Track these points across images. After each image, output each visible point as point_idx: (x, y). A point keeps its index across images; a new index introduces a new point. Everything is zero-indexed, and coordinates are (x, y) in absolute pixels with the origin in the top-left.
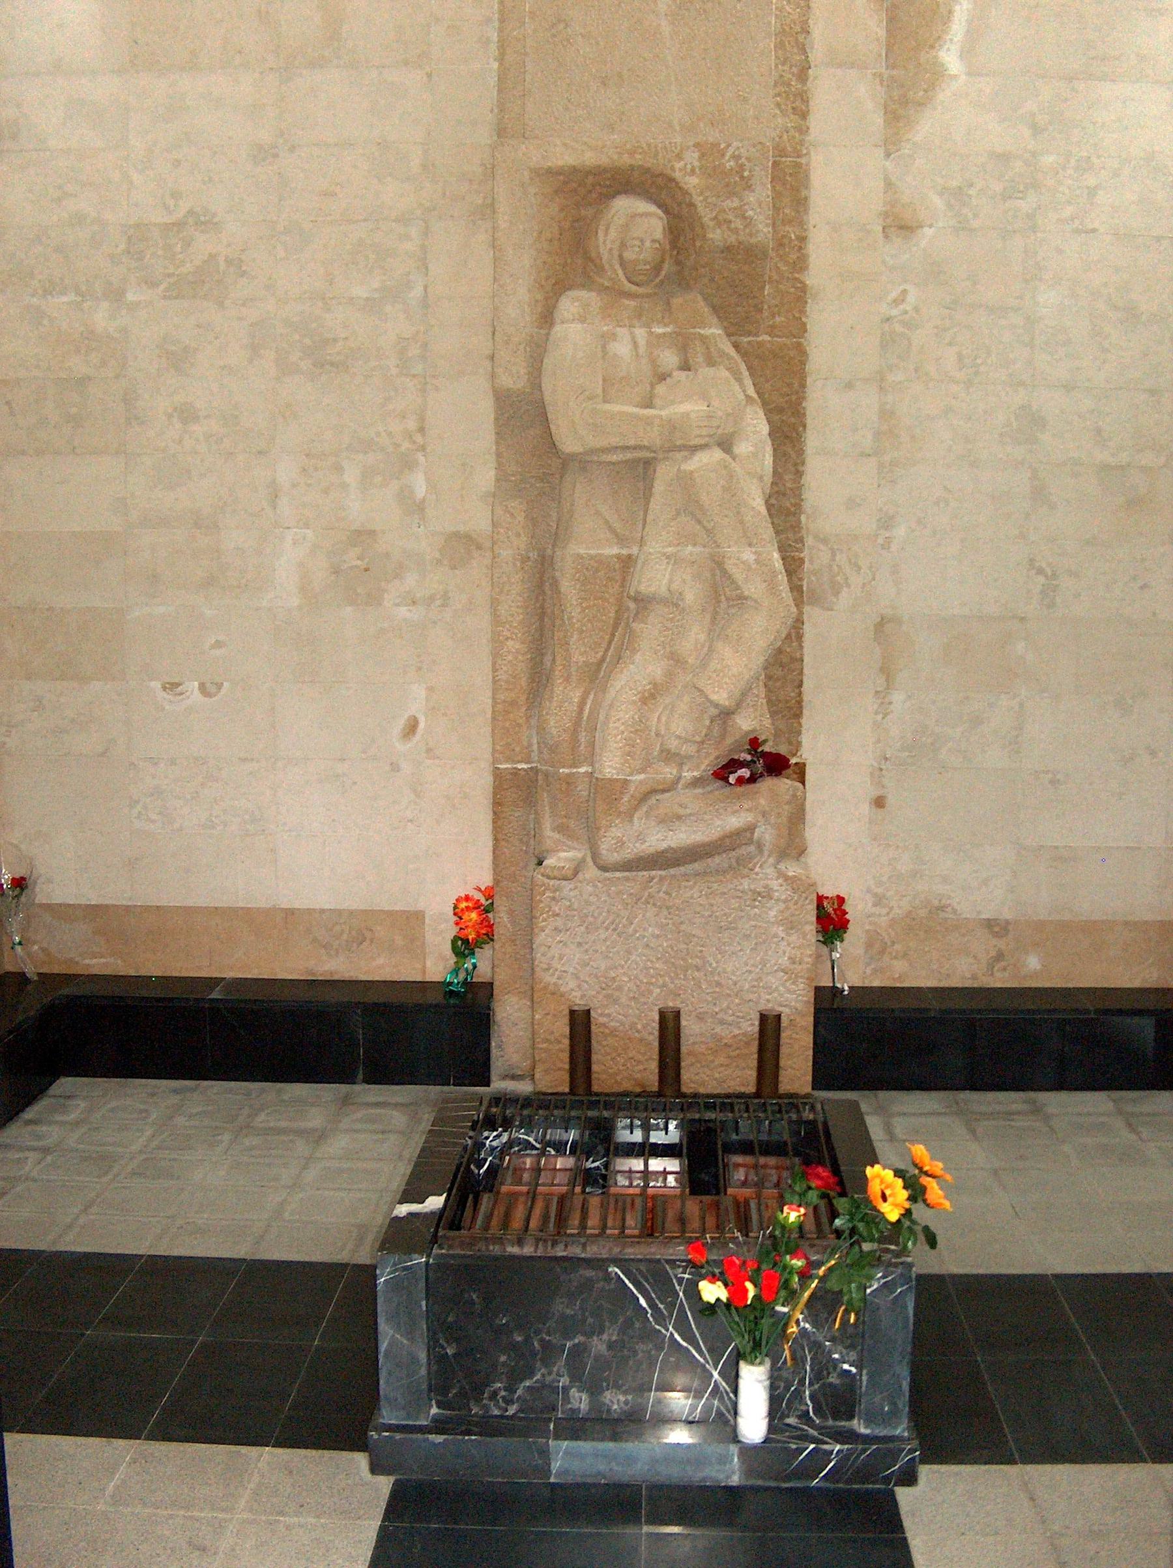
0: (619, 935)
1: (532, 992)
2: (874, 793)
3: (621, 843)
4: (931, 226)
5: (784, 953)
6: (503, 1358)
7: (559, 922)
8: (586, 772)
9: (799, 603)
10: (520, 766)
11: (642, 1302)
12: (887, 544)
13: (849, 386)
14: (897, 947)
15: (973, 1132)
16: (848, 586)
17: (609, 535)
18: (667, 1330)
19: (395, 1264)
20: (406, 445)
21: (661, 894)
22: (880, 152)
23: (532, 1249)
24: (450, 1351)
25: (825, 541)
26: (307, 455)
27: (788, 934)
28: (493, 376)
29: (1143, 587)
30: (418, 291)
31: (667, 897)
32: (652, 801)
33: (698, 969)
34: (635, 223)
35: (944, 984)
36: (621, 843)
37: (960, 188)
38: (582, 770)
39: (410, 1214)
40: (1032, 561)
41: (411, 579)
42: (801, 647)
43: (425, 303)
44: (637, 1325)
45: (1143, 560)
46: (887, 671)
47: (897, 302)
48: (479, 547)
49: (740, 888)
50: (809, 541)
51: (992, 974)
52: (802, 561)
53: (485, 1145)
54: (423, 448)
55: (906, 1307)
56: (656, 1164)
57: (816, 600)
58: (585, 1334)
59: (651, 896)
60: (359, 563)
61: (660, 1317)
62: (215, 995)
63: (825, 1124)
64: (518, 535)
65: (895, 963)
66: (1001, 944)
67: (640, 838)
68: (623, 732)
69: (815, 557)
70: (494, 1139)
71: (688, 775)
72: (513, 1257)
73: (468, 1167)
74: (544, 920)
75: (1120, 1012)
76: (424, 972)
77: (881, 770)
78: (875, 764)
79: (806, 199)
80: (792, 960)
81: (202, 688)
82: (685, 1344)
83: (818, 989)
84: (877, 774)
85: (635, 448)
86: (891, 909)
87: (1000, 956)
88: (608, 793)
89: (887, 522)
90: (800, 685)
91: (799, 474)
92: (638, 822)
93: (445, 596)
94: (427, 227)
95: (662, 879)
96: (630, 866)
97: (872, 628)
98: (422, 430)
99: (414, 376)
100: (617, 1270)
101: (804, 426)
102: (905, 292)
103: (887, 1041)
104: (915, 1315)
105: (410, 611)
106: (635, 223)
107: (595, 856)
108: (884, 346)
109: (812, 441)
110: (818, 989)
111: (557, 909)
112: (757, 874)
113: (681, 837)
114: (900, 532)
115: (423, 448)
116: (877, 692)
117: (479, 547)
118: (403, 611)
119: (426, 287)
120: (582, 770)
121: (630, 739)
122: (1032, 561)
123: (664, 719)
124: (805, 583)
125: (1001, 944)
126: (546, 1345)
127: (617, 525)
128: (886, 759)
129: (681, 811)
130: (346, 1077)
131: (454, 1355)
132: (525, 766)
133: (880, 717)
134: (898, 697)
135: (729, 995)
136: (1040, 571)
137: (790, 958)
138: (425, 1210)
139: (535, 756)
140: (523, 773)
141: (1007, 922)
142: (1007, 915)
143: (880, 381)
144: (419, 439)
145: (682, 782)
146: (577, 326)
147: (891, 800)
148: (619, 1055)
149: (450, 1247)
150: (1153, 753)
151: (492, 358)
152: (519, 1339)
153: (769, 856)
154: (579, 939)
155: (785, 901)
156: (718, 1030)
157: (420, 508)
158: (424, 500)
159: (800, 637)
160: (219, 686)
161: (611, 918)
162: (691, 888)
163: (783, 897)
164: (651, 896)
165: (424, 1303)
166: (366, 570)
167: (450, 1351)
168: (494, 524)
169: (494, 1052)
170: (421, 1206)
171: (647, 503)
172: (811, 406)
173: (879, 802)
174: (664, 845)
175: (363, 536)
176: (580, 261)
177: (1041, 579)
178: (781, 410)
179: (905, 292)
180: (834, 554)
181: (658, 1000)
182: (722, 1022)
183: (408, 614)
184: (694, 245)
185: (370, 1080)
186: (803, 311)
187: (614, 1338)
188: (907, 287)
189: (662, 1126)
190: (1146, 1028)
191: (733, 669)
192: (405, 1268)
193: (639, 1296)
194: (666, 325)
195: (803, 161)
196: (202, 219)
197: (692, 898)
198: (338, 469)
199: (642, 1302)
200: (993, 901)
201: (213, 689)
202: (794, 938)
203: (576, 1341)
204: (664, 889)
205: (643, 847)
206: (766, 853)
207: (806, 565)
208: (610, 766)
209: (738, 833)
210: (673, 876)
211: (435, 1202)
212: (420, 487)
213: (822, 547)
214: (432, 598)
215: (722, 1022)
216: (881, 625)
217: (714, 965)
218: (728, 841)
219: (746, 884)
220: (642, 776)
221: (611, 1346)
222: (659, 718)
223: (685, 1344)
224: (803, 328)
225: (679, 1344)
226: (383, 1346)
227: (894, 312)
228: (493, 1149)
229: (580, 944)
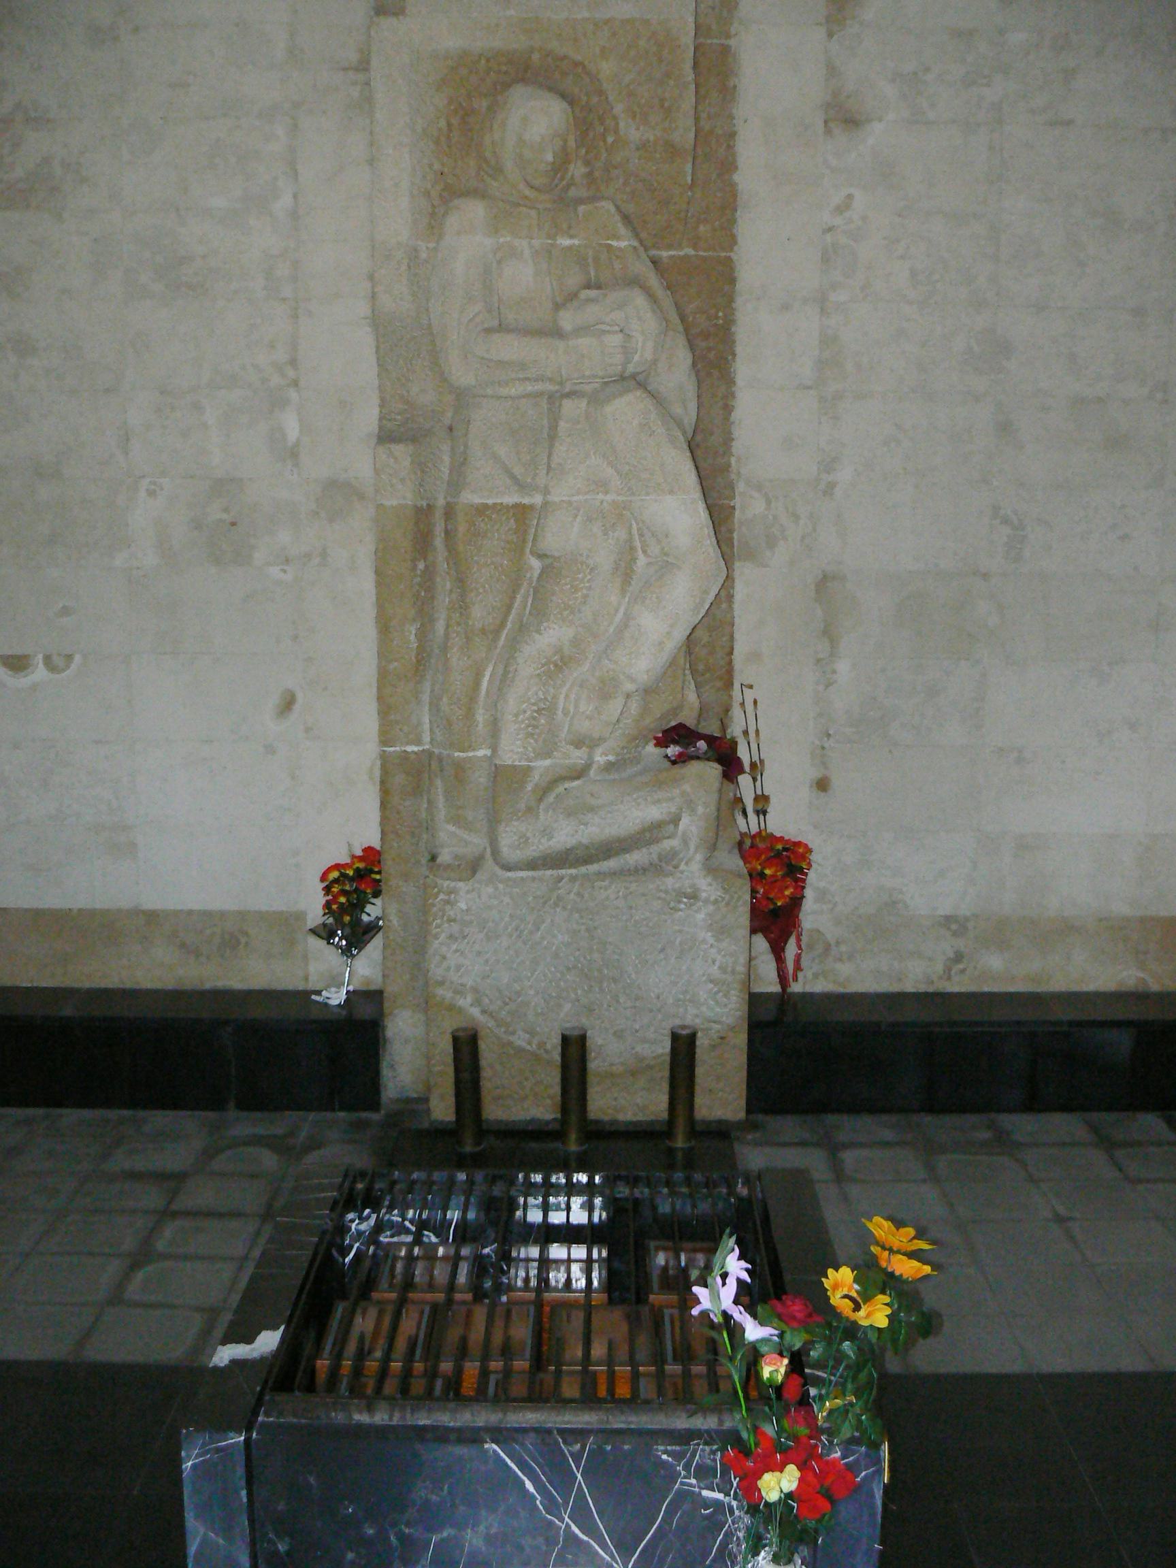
0: (525, 943)
1: (427, 1004)
2: (815, 774)
3: (524, 840)
4: (880, 120)
5: (714, 962)
6: (350, 1556)
7: (455, 928)
8: (485, 756)
9: (728, 559)
10: (410, 749)
11: (529, 1486)
12: (830, 489)
13: (786, 307)
14: (843, 948)
15: (930, 1167)
16: (785, 539)
17: (508, 481)
18: (562, 1520)
19: (204, 1444)
20: (276, 380)
21: (572, 896)
22: (821, 33)
23: (386, 1417)
24: (282, 1547)
25: (759, 488)
26: (162, 393)
27: (718, 940)
28: (373, 296)
29: (1124, 538)
30: (286, 201)
31: (578, 900)
32: (560, 789)
33: (615, 980)
34: (534, 122)
35: (895, 988)
36: (524, 840)
37: (915, 73)
38: (480, 753)
39: (235, 1363)
40: (996, 509)
41: (284, 537)
42: (731, 608)
43: (294, 215)
44: (523, 1514)
45: (1123, 506)
46: (829, 633)
47: (840, 210)
48: (362, 497)
49: (662, 888)
50: (741, 487)
51: (949, 978)
52: (734, 508)
53: (350, 1228)
54: (295, 383)
55: (873, 1496)
56: (557, 1251)
57: (750, 555)
58: (454, 1525)
59: (559, 898)
60: (225, 516)
61: (552, 1506)
62: (67, 1011)
63: (764, 1203)
64: (403, 480)
65: (838, 966)
66: (960, 943)
67: (547, 833)
68: (525, 712)
69: (749, 507)
70: (359, 1224)
71: (600, 758)
72: (360, 1426)
73: (328, 1250)
74: (438, 926)
75: (1103, 1024)
76: (306, 979)
77: (823, 748)
78: (817, 742)
79: (735, 87)
80: (723, 969)
81: (48, 660)
82: (585, 1538)
83: (755, 1000)
84: (820, 754)
85: (536, 380)
86: (835, 904)
87: (958, 957)
88: (506, 779)
89: (829, 464)
90: (731, 653)
91: (728, 409)
92: (544, 817)
93: (324, 554)
94: (296, 126)
95: (573, 879)
96: (532, 865)
97: (813, 587)
98: (293, 362)
99: (284, 299)
100: (495, 1446)
101: (734, 355)
102: (850, 197)
103: (833, 1061)
104: (885, 1505)
105: (285, 571)
106: (534, 122)
107: (495, 853)
108: (826, 259)
109: (742, 370)
110: (755, 1000)
111: (452, 913)
112: (682, 872)
113: (594, 830)
114: (844, 475)
115: (295, 383)
116: (819, 661)
117: (362, 497)
118: (275, 572)
119: (295, 196)
120: (480, 753)
121: (534, 718)
122: (996, 509)
123: (573, 696)
124: (735, 535)
125: (960, 943)
126: (405, 1540)
127: (518, 470)
128: (829, 735)
129: (593, 802)
130: (216, 1102)
131: (289, 1554)
132: (416, 749)
133: (821, 688)
134: (843, 667)
135: (651, 1011)
136: (1005, 521)
137: (720, 968)
138: (256, 1355)
139: (426, 738)
140: (413, 756)
141: (967, 919)
142: (964, 911)
143: (821, 301)
144: (291, 373)
145: (595, 766)
146: (470, 237)
147: (836, 782)
148: (526, 1079)
149: (281, 1414)
150: (1133, 726)
151: (371, 278)
152: (371, 1532)
153: (696, 852)
154: (477, 947)
155: (716, 902)
156: (639, 1049)
157: (294, 453)
158: (297, 444)
159: (730, 598)
160: (69, 658)
161: (514, 924)
162: (606, 889)
163: (712, 898)
164: (559, 898)
165: (244, 1493)
166: (233, 524)
167: (282, 1547)
168: (377, 472)
169: (385, 1072)
170: (248, 1347)
171: (551, 446)
172: (741, 332)
173: (822, 785)
174: (571, 842)
175: (224, 486)
176: (472, 163)
177: (1006, 530)
178: (706, 336)
179: (850, 197)
180: (768, 502)
181: (566, 1018)
182: (644, 1040)
183: (282, 575)
184: (605, 141)
185: (243, 1105)
186: (733, 221)
187: (493, 1531)
188: (852, 190)
189: (563, 1206)
190: (1124, 1042)
191: (653, 635)
192: (218, 1450)
193: (525, 1478)
194: (571, 237)
195: (732, 42)
196: (33, 115)
197: (607, 898)
198: (197, 407)
199: (529, 1486)
200: (952, 896)
201: (59, 661)
202: (724, 945)
203: (445, 1534)
204: (575, 890)
205: (551, 843)
206: (692, 848)
207: (737, 513)
208: (512, 751)
209: (659, 825)
210: (586, 877)
211: (268, 1341)
212: (292, 429)
213: (756, 494)
214: (308, 556)
215: (644, 1040)
216: (825, 584)
217: (633, 976)
218: (648, 835)
219: (669, 881)
220: (547, 762)
221: (490, 1539)
222: (567, 697)
223: (585, 1538)
224: (733, 241)
225: (576, 1536)
226: (192, 1549)
227: (838, 221)
228: (360, 1234)
229: (479, 953)
